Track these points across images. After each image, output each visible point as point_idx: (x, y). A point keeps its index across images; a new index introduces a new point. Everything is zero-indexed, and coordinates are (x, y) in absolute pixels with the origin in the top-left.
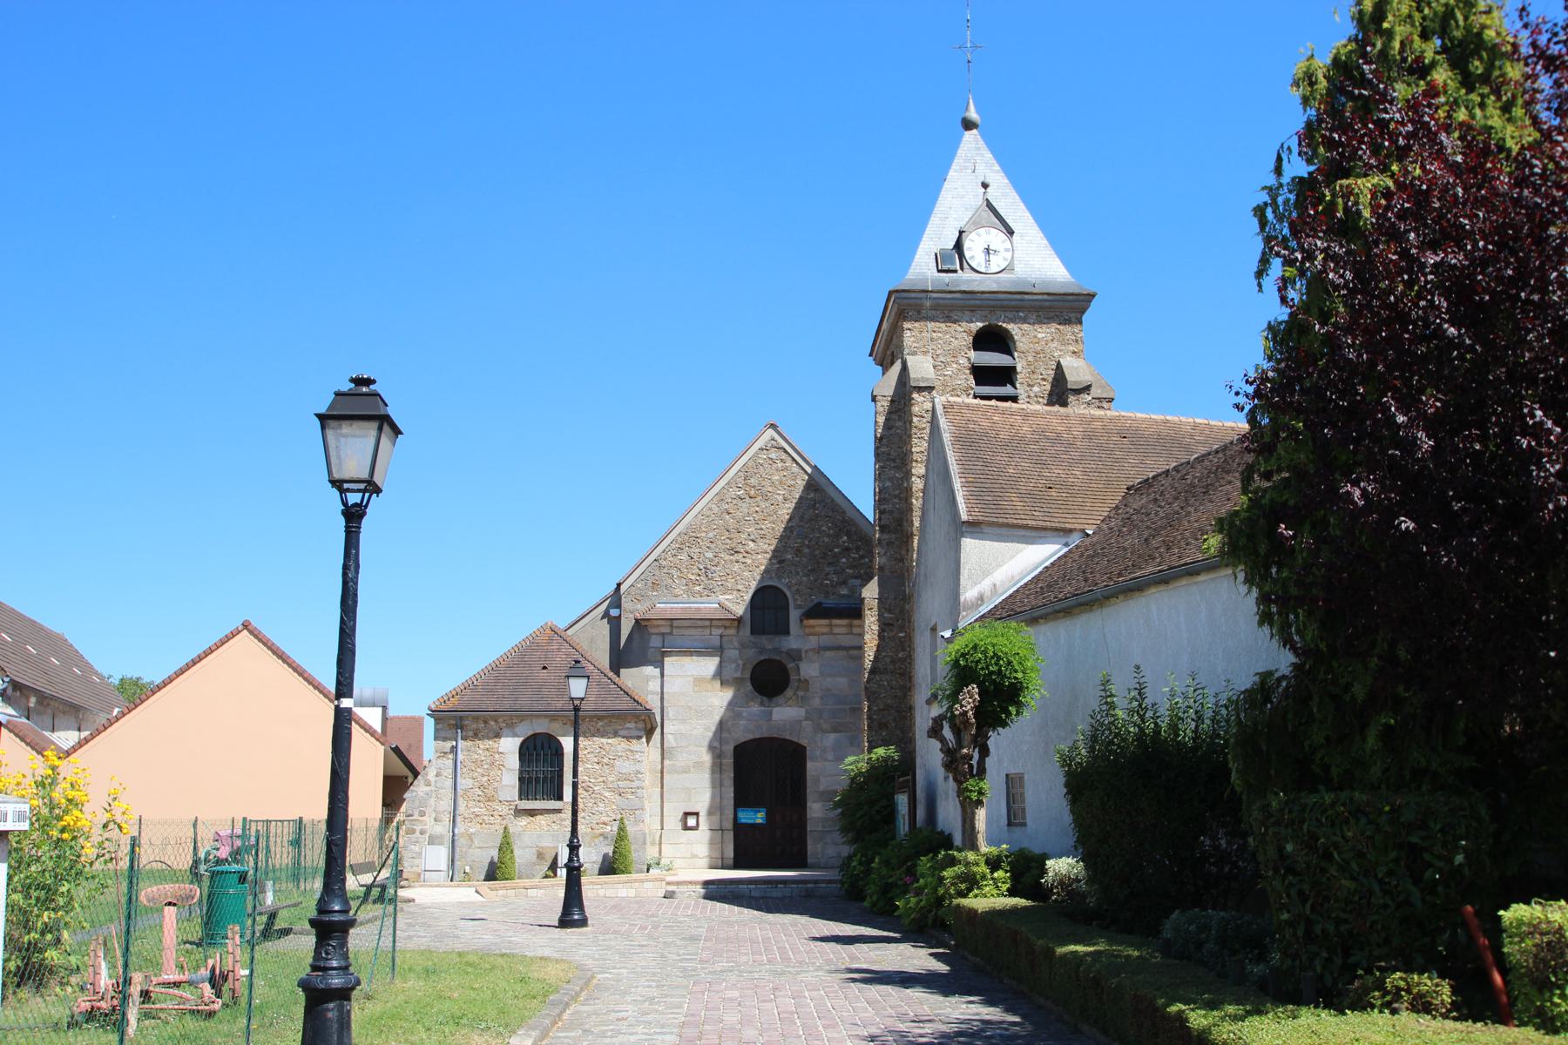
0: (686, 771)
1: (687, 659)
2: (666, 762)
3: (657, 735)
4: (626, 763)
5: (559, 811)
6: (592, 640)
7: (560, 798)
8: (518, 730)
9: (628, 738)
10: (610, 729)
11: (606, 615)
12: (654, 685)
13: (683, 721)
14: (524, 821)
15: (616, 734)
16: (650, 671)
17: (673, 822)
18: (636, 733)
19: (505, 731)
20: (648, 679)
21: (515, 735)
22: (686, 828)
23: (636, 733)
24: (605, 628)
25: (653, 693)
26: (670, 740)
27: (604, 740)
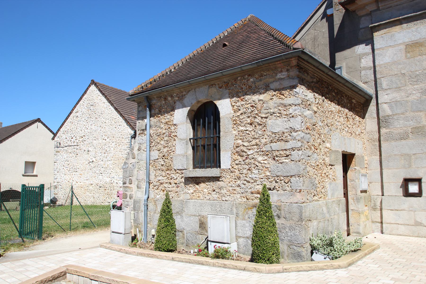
0: (404, 137)
1: (397, 29)
2: (383, 131)
3: (372, 107)
4: (279, 121)
5: (217, 179)
6: (315, 39)
7: (217, 164)
8: (186, 100)
9: (279, 90)
10: (260, 84)
11: (324, 15)
12: (367, 62)
13: (398, 89)
14: (191, 188)
15: (267, 88)
16: (362, 49)
17: (394, 188)
18: (287, 83)
19: (178, 103)
20: (360, 57)
21: (184, 106)
22: (407, 194)
23: (287, 83)
24: (325, 24)
25: (365, 69)
26: (385, 110)
27: (256, 97)
